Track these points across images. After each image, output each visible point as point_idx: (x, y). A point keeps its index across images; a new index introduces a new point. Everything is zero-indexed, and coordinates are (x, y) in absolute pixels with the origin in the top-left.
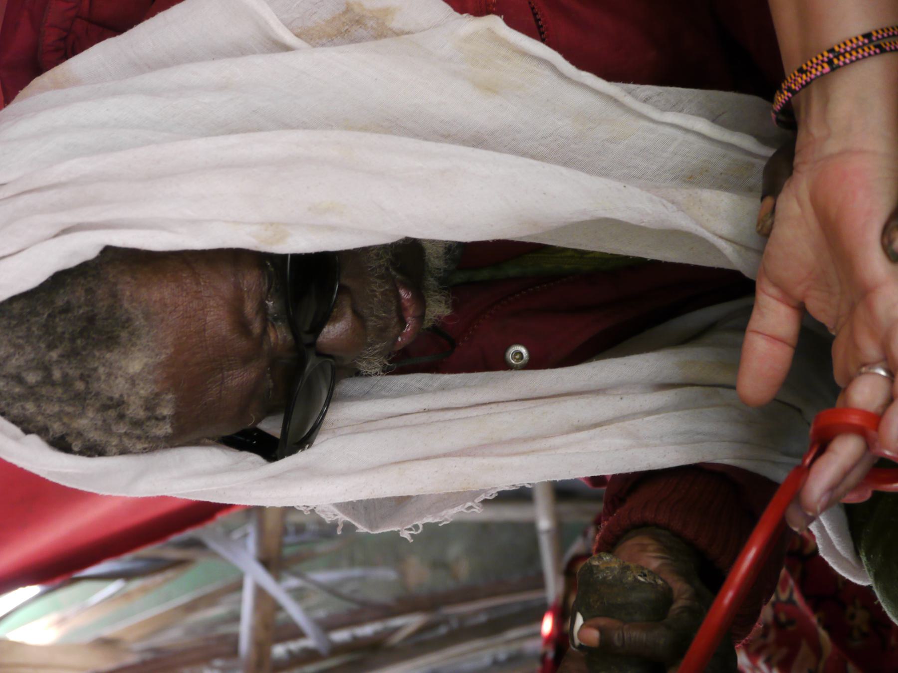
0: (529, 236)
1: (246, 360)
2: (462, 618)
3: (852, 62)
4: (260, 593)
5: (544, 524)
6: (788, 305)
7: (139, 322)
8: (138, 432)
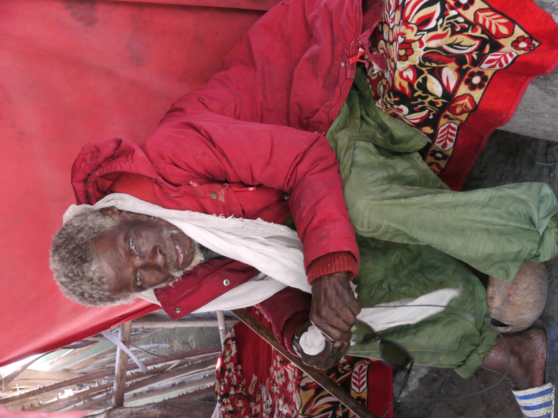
2: (193, 361)
4: (122, 352)
5: (221, 328)
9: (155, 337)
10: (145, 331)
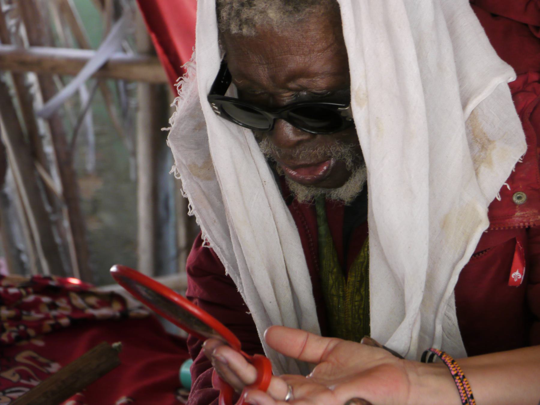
0: (372, 211)
1: (273, 78)
2: (58, 224)
3: (457, 387)
4: (81, 63)
6: (323, 355)
7: (298, 17)
8: (233, 14)
9: (113, 135)
10: (126, 114)
